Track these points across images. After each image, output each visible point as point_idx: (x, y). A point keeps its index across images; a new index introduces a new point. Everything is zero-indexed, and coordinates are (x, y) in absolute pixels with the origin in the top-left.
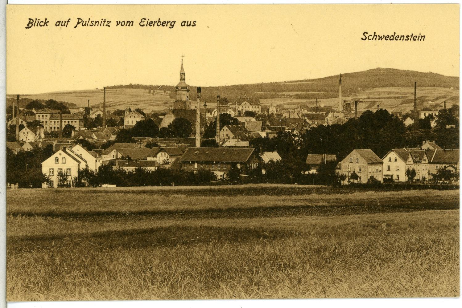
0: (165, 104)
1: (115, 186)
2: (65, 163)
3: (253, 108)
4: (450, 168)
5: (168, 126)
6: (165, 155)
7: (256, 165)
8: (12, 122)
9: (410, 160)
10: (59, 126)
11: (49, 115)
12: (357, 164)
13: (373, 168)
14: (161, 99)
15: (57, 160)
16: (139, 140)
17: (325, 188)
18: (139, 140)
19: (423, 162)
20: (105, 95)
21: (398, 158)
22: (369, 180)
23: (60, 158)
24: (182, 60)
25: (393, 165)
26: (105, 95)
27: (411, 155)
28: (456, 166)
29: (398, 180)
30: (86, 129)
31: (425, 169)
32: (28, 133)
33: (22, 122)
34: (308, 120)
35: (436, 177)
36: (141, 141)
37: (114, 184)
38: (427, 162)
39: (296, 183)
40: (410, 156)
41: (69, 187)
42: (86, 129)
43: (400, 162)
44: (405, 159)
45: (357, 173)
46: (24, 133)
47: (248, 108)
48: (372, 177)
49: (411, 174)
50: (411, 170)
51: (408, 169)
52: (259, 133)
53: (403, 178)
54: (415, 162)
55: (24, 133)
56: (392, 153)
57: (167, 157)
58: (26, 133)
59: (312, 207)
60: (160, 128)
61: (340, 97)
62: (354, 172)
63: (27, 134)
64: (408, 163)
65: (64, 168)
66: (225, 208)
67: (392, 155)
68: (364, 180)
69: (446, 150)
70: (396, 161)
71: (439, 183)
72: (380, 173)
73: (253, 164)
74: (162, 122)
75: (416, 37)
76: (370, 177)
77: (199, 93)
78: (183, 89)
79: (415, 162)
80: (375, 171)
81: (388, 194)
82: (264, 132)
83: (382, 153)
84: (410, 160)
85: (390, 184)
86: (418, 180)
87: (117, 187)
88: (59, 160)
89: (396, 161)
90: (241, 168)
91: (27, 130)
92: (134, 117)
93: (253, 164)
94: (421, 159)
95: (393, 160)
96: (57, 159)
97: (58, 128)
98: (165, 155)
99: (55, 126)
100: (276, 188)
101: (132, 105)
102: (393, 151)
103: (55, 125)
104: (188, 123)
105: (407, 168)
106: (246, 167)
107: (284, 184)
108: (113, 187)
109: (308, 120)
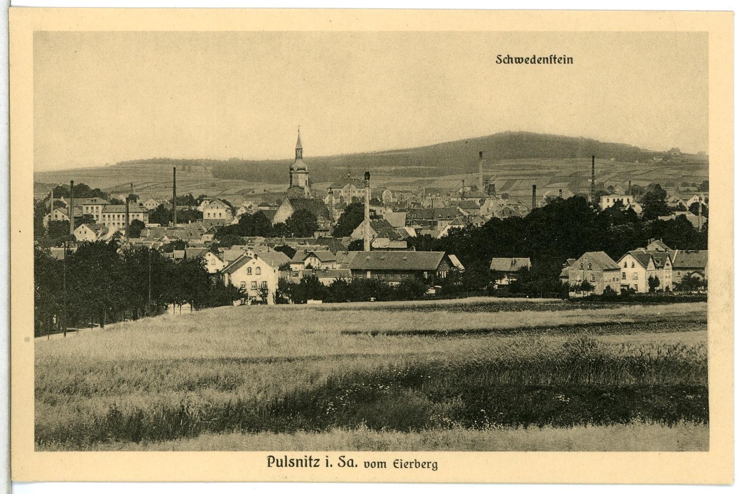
0: (212, 186)
1: (321, 302)
2: (260, 274)
3: (359, 192)
4: (696, 275)
5: (286, 221)
6: (315, 261)
7: (447, 273)
8: (50, 216)
9: (651, 264)
10: (124, 222)
11: (100, 207)
12: (590, 271)
13: (608, 276)
14: (476, 210)
15: (249, 271)
16: (249, 241)
17: (560, 302)
18: (249, 241)
19: (666, 267)
20: (174, 179)
21: (636, 262)
22: (605, 291)
23: (254, 267)
24: (299, 131)
25: (629, 271)
26: (174, 179)
27: (653, 259)
28: (703, 272)
29: (637, 291)
30: (158, 226)
31: (668, 277)
32: (85, 232)
33: (63, 216)
34: (461, 210)
35: (678, 287)
36: (251, 242)
37: (318, 300)
38: (670, 266)
39: (372, 299)
40: (651, 259)
41: (704, 301)
42: (160, 225)
43: (639, 268)
44: (645, 265)
45: (590, 283)
46: (80, 232)
47: (354, 192)
48: (608, 287)
49: (653, 282)
50: (654, 277)
51: (651, 276)
52: (405, 230)
53: (643, 287)
54: (657, 268)
55: (80, 232)
56: (628, 256)
57: (318, 264)
58: (83, 232)
59: (617, 324)
60: (273, 224)
61: (481, 172)
62: (586, 280)
63: (628, 264)
64: (648, 269)
65: (260, 280)
66: (533, 326)
67: (628, 259)
68: (599, 291)
69: (689, 251)
70: (633, 266)
71: (693, 294)
72: (617, 282)
73: (443, 272)
74: (276, 216)
75: (561, 58)
76: (606, 287)
77: (367, 180)
78: (300, 171)
79: (657, 268)
80: (612, 280)
81: (625, 309)
82: (411, 228)
83: (617, 255)
84: (651, 264)
85: (629, 296)
86: (661, 291)
87: (324, 304)
88: (252, 270)
89: (633, 266)
90: (430, 278)
91: (84, 229)
92: (217, 208)
93: (443, 272)
94: (663, 263)
95: (629, 265)
96: (250, 269)
97: (123, 224)
98: (315, 261)
99: (119, 222)
100: (505, 303)
101: (167, 189)
102: (629, 253)
103: (119, 220)
104: (310, 215)
105: (648, 277)
106: (435, 276)
107: (478, 296)
108: (319, 303)
109: (461, 210)
